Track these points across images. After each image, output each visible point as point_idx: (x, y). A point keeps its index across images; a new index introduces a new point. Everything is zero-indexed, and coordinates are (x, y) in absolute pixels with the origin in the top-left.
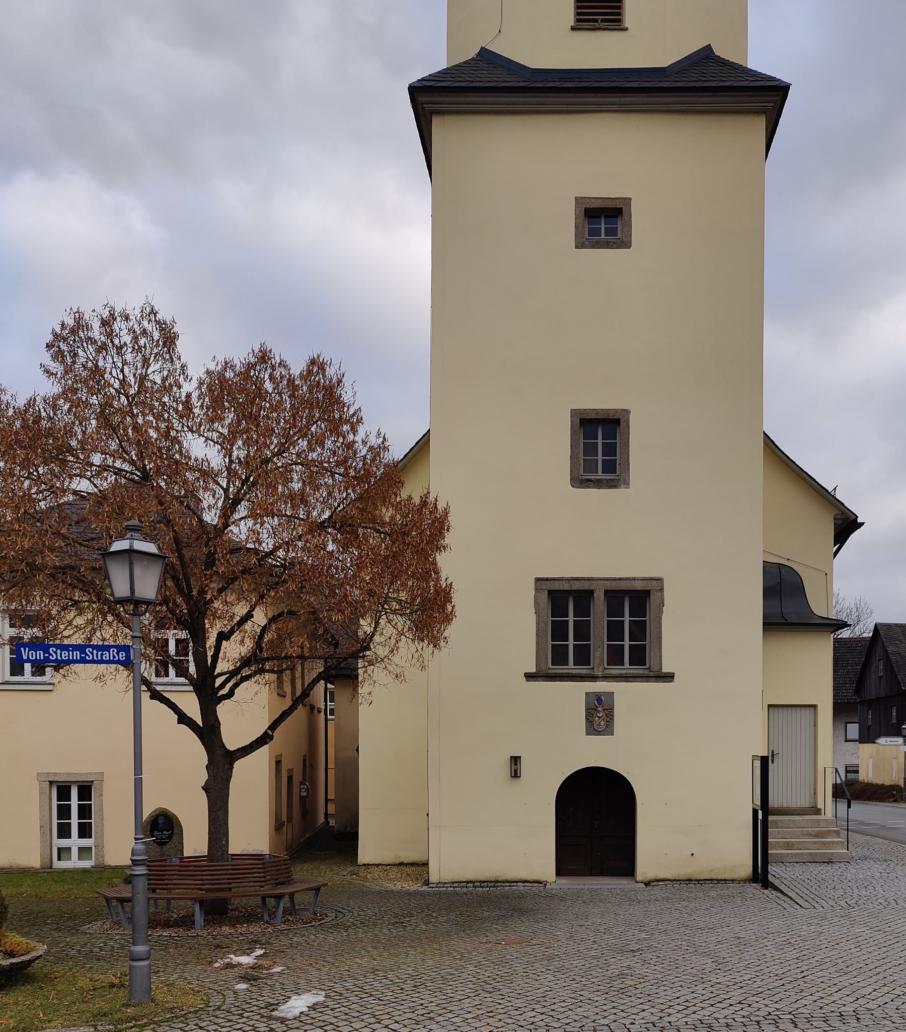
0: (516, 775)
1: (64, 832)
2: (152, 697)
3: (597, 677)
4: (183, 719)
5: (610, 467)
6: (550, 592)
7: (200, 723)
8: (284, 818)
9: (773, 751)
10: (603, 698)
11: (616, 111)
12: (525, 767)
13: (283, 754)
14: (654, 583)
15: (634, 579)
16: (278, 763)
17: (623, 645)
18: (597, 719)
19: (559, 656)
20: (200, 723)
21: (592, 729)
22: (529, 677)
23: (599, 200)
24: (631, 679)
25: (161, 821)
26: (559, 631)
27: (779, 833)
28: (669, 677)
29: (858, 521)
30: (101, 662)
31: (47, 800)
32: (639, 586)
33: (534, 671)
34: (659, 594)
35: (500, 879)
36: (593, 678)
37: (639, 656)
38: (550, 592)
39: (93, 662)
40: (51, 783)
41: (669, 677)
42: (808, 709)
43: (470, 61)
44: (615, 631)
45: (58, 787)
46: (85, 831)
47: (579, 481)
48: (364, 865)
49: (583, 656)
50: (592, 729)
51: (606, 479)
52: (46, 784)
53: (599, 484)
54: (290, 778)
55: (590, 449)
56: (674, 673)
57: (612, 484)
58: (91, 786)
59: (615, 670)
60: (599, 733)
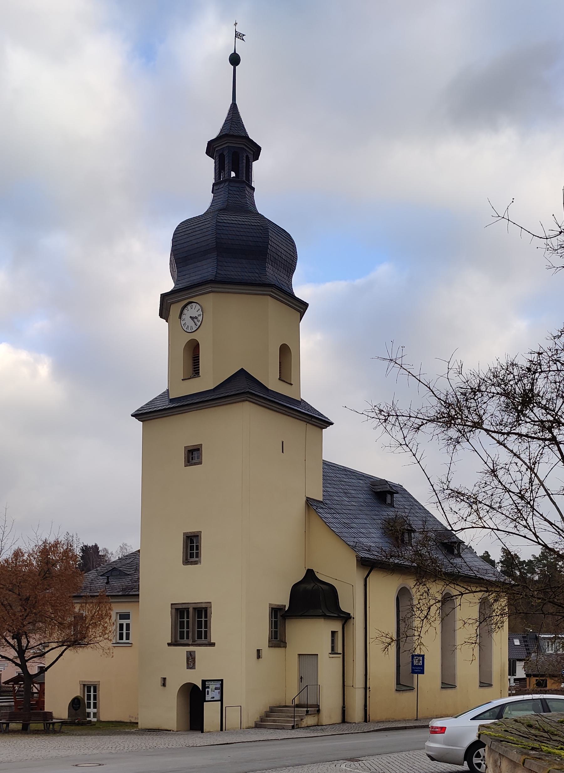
3: (190, 645)
9: (301, 676)
11: (235, 403)
12: (159, 682)
15: (202, 603)
22: (169, 644)
24: (201, 645)
25: (76, 700)
29: (205, 703)
34: (210, 609)
35: (160, 729)
36: (188, 645)
37: (207, 635)
41: (213, 645)
43: (149, 403)
46: (95, 707)
52: (305, 702)
56: (215, 643)
59: (199, 641)
60: (191, 668)
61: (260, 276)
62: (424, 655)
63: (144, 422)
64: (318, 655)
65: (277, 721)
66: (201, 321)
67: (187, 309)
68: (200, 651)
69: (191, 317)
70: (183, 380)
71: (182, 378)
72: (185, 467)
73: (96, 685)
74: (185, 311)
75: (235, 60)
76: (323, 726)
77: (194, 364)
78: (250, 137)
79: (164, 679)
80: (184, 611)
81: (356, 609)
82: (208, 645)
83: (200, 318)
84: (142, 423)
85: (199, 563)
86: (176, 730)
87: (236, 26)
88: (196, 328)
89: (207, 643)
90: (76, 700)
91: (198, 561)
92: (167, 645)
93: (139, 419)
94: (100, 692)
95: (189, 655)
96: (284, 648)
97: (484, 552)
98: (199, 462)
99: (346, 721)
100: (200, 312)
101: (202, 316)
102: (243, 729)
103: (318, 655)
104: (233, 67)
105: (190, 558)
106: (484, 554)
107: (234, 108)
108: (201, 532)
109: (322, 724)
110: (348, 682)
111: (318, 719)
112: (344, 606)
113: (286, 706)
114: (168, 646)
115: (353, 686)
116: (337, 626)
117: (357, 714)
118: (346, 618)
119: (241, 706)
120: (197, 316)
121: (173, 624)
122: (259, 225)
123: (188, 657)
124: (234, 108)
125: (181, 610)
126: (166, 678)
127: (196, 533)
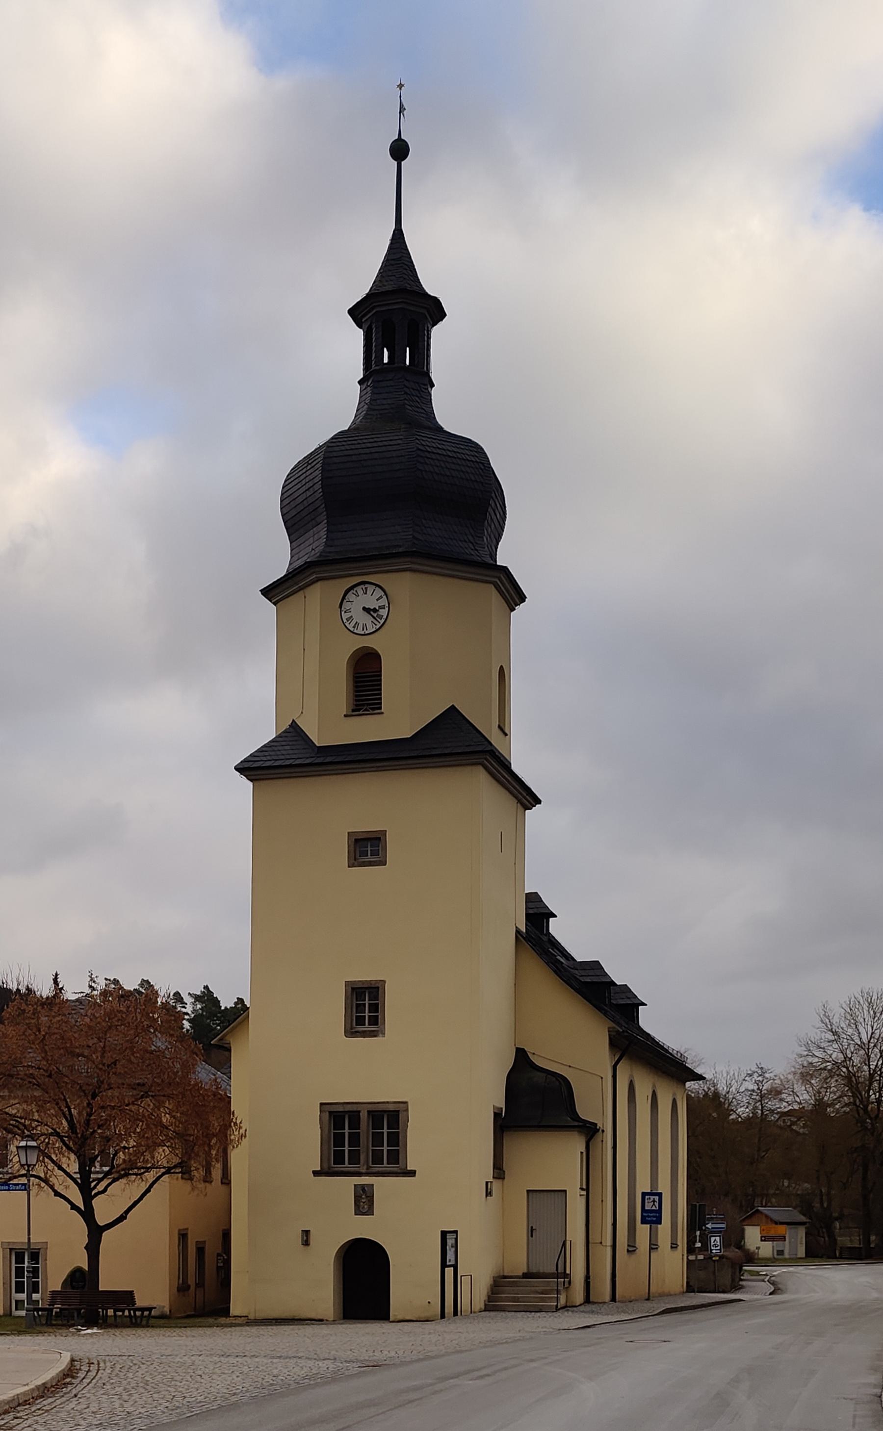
0: (306, 1243)
1: (20, 1288)
2: (55, 1195)
4: (74, 1207)
5: (374, 1021)
6: (330, 1113)
7: (83, 1209)
8: (191, 1281)
9: (532, 1227)
10: (366, 1188)
13: (190, 1228)
14: (402, 1105)
16: (183, 1236)
17: (388, 1146)
18: (362, 1204)
19: (339, 1158)
20: (83, 1209)
21: (359, 1211)
22: (316, 1173)
23: (364, 833)
24: (386, 1175)
25: (78, 1274)
26: (339, 1140)
27: (513, 1290)
28: (412, 1173)
30: (16, 1190)
31: (8, 1262)
32: (391, 1108)
33: (319, 1169)
34: (405, 1113)
36: (359, 1174)
38: (330, 1113)
39: (12, 1190)
40: (11, 1249)
41: (412, 1173)
42: (553, 1193)
44: (377, 1139)
45: (16, 1253)
47: (351, 1032)
48: (234, 1317)
49: (355, 1158)
50: (359, 1211)
51: (369, 1031)
53: (364, 1034)
54: (201, 1250)
55: (360, 1008)
57: (374, 1034)
58: (39, 1253)
59: (377, 1168)
61: (477, 548)
62: (661, 1194)
63: (257, 783)
64: (565, 1191)
65: (520, 1300)
66: (385, 617)
67: (355, 592)
68: (383, 1186)
69: (364, 609)
70: (345, 716)
71: (345, 713)
72: (349, 867)
73: (39, 1249)
74: (351, 596)
75: (400, 150)
76: (576, 1306)
77: (355, 689)
78: (429, 293)
79: (306, 1233)
80: (344, 1116)
81: (607, 1116)
82: (401, 1175)
83: (384, 612)
84: (250, 784)
85: (381, 1035)
86: (332, 1319)
87: (400, 89)
88: (374, 630)
89: (399, 1171)
90: (78, 1274)
91: (378, 1031)
92: (312, 1175)
93: (250, 775)
94: (48, 1262)
95: (361, 1192)
96: (501, 1180)
97: (236, 1000)
98: (380, 861)
99: (591, 1300)
100: (384, 601)
101: (387, 609)
102: (475, 1312)
103: (565, 1191)
104: (396, 163)
105: (356, 1025)
106: (236, 1003)
107: (398, 237)
108: (384, 982)
109: (574, 1305)
110: (594, 1237)
111: (567, 1296)
112: (585, 1112)
113: (503, 1276)
114: (314, 1176)
115: (601, 1243)
116: (575, 1144)
117: (603, 1289)
118: (590, 1131)
119: (471, 1276)
120: (377, 608)
121: (324, 1136)
122: (478, 461)
123: (358, 1194)
124: (398, 237)
125: (335, 1114)
126: (309, 1231)
127: (373, 983)
